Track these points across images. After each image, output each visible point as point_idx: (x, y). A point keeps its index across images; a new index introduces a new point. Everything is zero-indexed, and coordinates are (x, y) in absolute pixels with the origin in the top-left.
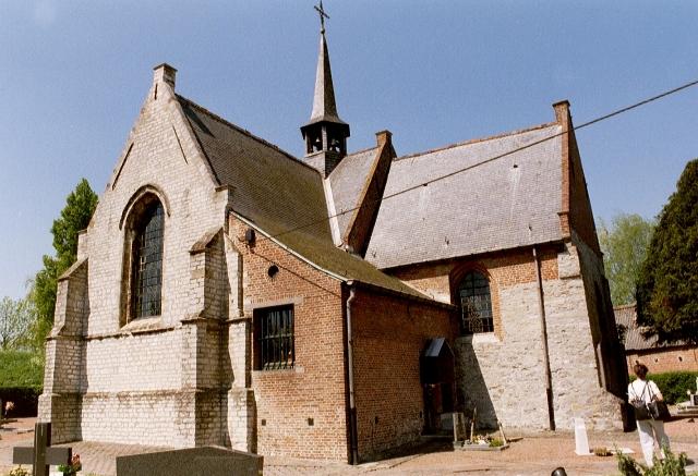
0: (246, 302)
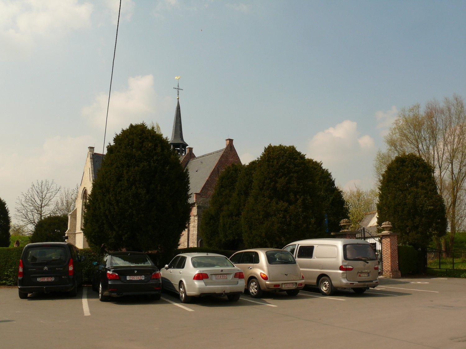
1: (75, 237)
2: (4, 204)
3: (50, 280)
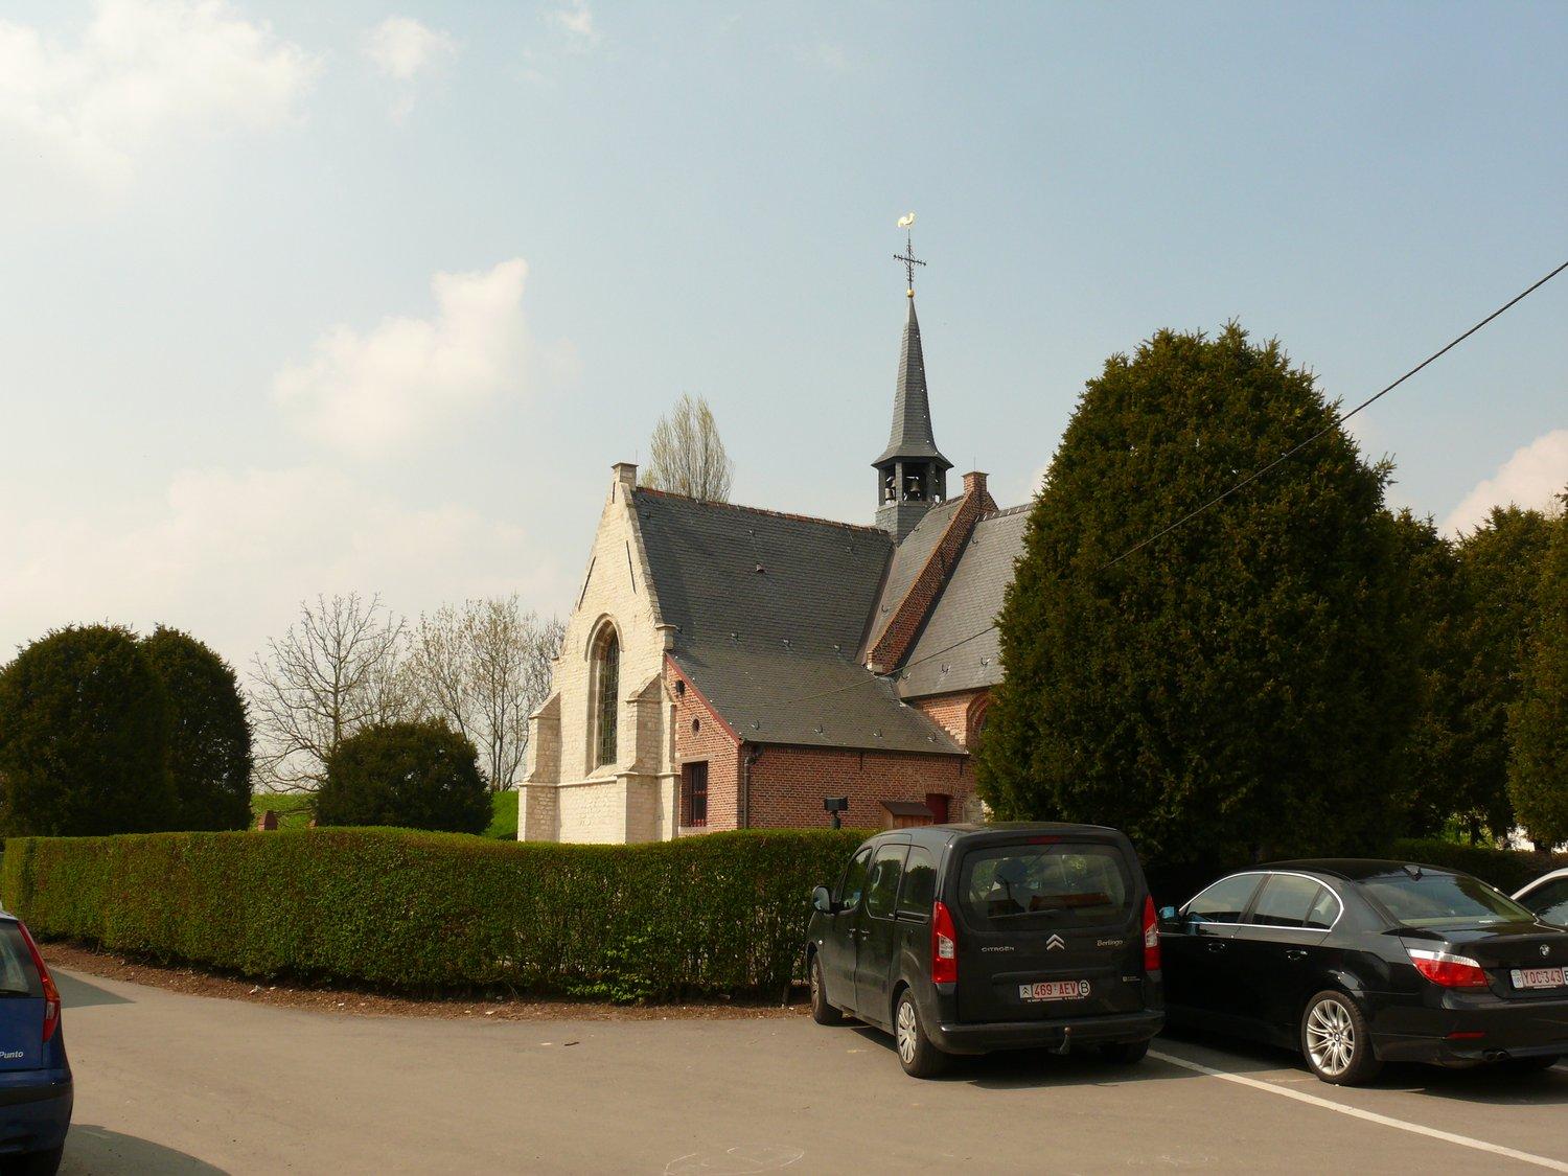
0: (677, 755)
1: (555, 800)
2: (230, 678)
3: (1072, 994)
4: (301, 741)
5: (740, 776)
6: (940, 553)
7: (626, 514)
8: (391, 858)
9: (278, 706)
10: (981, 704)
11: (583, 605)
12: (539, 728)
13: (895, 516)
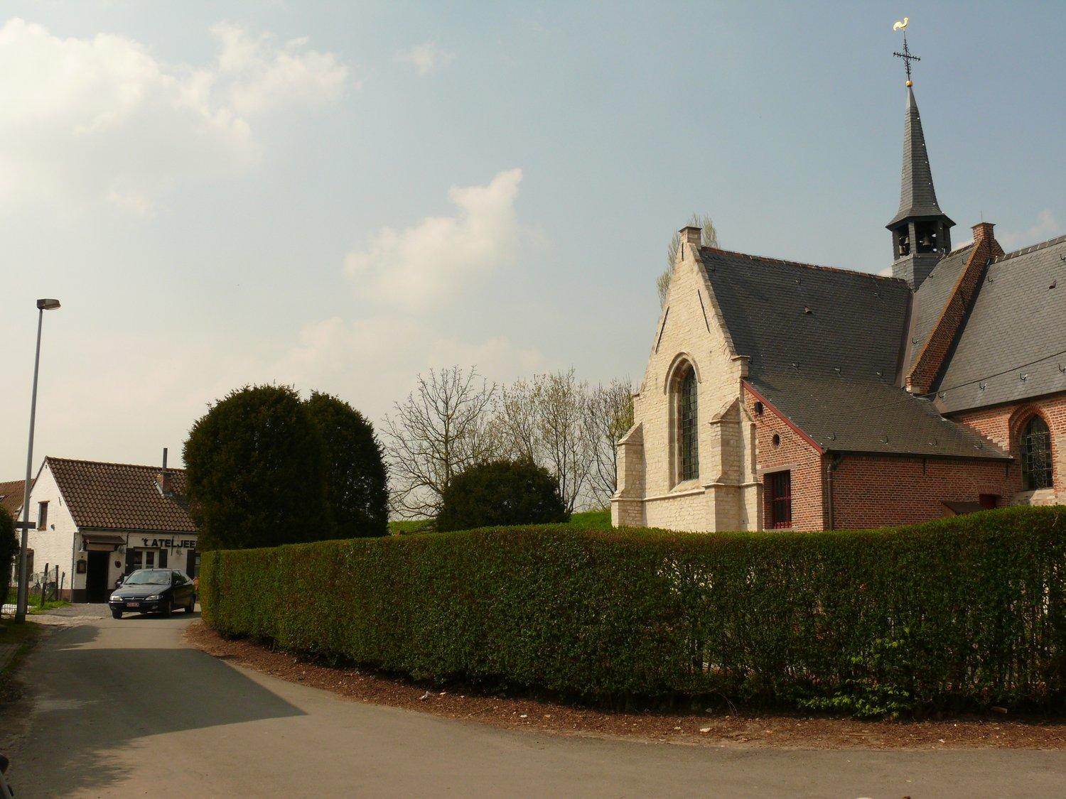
0: (758, 467)
4: (423, 479)
5: (824, 481)
6: (960, 292)
7: (696, 268)
8: (574, 556)
9: (403, 453)
10: (1023, 413)
11: (660, 348)
12: (626, 453)
13: (911, 266)
